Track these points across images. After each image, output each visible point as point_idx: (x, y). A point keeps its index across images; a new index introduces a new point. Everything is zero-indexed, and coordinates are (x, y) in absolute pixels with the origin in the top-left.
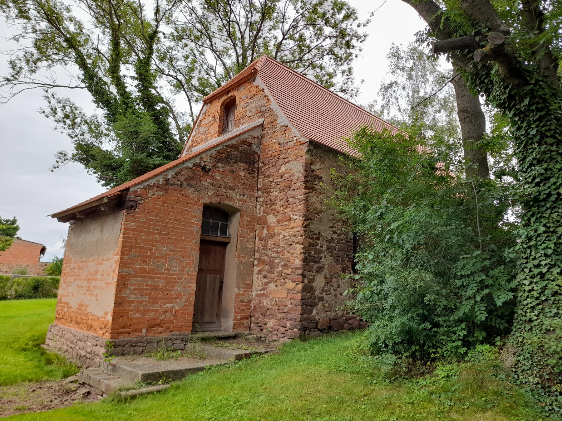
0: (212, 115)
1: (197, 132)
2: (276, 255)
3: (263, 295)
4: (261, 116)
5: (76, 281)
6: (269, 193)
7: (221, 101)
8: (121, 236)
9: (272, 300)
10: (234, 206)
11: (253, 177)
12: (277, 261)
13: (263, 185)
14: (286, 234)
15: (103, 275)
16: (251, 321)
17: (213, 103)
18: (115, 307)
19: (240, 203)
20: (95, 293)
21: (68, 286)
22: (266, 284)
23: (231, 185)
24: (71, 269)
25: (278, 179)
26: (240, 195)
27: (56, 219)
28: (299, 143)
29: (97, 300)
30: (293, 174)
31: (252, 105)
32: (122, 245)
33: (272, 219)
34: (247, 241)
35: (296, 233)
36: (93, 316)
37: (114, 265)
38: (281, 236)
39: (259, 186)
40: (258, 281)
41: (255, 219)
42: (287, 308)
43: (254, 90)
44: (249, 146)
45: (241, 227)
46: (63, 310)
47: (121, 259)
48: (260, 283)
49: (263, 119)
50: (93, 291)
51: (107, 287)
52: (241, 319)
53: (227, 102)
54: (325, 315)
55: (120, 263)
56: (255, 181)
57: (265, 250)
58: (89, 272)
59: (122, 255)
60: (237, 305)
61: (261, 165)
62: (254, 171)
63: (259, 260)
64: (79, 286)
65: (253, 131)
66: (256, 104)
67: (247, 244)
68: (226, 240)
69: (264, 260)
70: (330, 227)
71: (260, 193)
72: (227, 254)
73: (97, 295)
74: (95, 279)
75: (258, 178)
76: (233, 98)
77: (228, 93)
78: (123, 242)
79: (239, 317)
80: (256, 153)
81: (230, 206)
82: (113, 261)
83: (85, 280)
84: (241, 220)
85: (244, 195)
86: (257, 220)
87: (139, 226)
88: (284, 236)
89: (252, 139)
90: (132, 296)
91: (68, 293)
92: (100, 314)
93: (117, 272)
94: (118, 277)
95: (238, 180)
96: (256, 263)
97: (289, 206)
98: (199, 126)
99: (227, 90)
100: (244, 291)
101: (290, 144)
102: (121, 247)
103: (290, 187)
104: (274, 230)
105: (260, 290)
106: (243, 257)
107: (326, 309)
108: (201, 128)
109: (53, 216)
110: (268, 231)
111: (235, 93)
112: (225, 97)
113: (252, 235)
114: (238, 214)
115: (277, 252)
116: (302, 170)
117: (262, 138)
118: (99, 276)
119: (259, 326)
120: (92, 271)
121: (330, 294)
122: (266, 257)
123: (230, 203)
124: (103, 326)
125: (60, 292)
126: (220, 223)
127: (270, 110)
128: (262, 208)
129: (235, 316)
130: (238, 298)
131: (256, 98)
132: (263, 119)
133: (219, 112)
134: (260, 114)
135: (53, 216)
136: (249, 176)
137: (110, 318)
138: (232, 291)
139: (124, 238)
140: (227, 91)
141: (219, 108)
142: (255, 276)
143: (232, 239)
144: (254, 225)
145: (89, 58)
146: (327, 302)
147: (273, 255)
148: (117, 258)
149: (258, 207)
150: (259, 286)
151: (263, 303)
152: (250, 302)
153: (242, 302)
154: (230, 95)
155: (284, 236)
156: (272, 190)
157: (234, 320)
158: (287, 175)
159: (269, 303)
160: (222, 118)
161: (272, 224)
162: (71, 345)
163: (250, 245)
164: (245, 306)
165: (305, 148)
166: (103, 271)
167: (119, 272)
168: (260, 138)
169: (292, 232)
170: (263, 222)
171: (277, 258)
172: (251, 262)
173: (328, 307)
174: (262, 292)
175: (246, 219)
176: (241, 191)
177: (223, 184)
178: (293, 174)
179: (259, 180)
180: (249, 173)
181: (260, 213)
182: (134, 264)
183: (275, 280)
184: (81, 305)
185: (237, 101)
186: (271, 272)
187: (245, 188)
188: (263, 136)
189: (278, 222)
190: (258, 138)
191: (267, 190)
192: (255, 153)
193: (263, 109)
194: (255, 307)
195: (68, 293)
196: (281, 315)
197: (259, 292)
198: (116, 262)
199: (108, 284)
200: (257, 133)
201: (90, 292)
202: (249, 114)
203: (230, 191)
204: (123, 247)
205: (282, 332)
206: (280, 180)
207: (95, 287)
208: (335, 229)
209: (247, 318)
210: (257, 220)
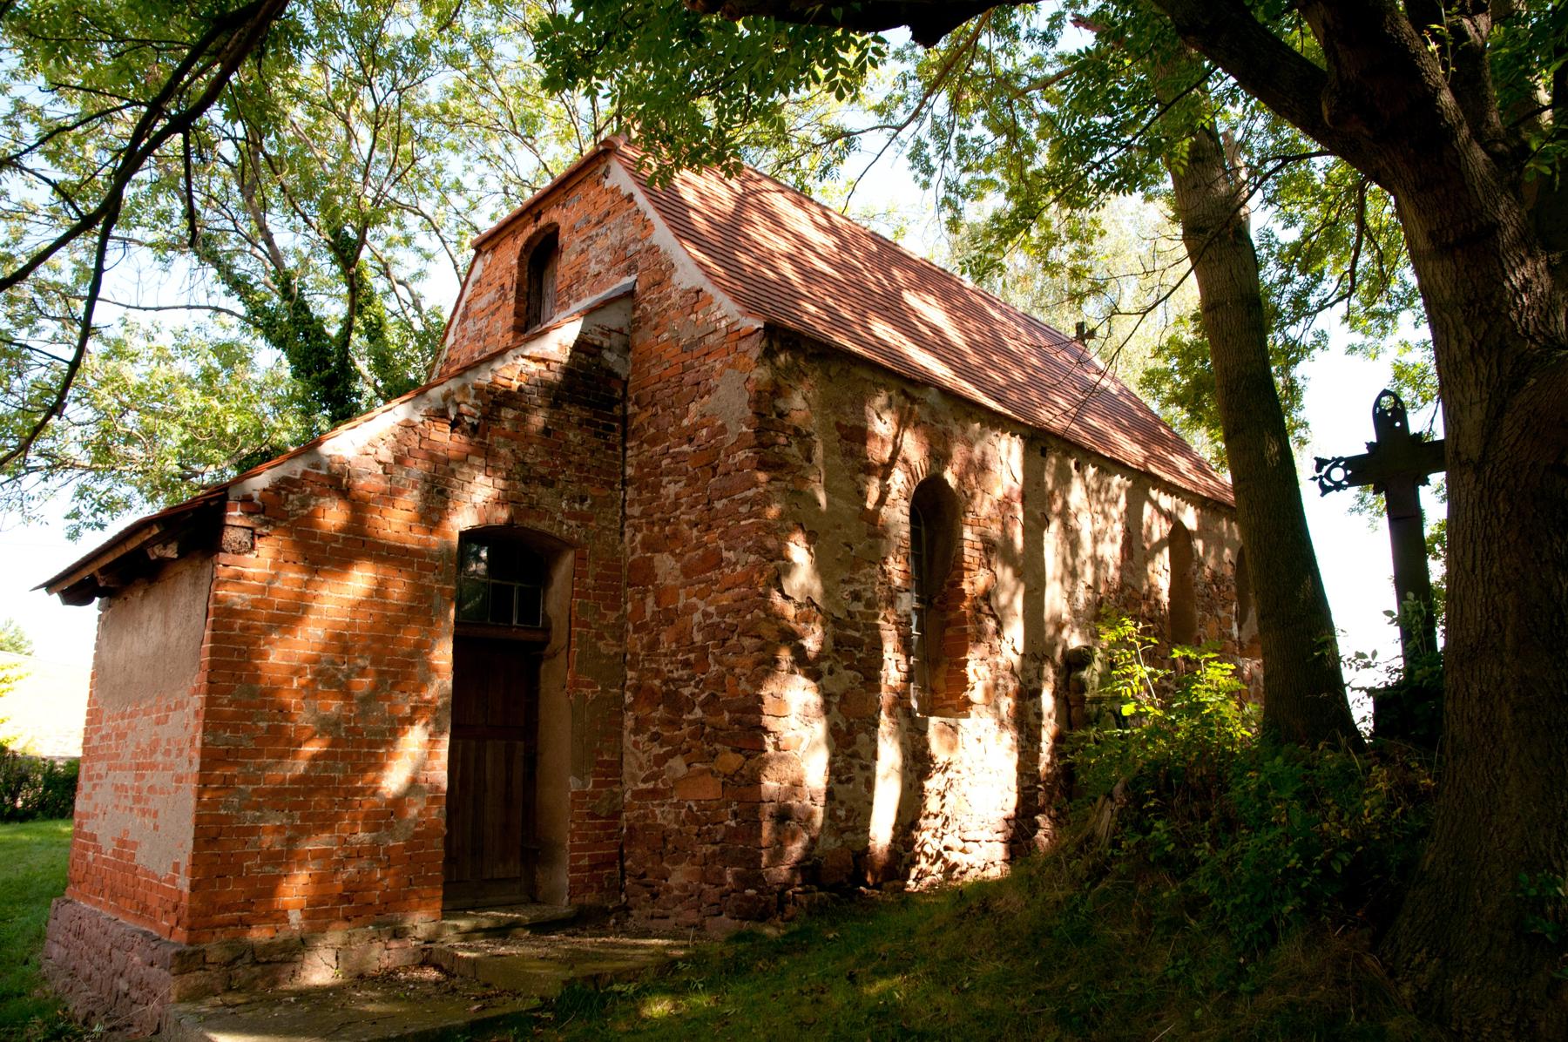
0: (497, 284)
1: (459, 335)
2: (684, 673)
3: (654, 793)
4: (628, 272)
5: (112, 773)
6: (656, 487)
7: (520, 242)
8: (208, 633)
9: (678, 805)
10: (555, 531)
11: (613, 447)
12: (686, 692)
13: (640, 467)
14: (711, 609)
15: (167, 753)
16: (623, 869)
17: (499, 251)
18: (196, 847)
19: (573, 523)
20: (152, 806)
21: (94, 786)
22: (661, 760)
23: (543, 470)
24: (102, 738)
25: (680, 445)
26: (572, 499)
27: (56, 597)
28: (734, 337)
29: (156, 828)
30: (723, 429)
31: (602, 242)
32: (211, 662)
33: (666, 565)
34: (600, 637)
35: (738, 605)
36: (147, 874)
37: (193, 722)
38: (697, 617)
39: (630, 471)
40: (637, 753)
41: (619, 568)
42: (721, 828)
43: (605, 203)
44: (593, 356)
45: (578, 595)
46: (84, 856)
47: (210, 701)
48: (644, 758)
49: (634, 277)
50: (147, 801)
51: (177, 788)
52: (592, 867)
53: (536, 243)
54: (839, 843)
55: (207, 715)
56: (617, 458)
57: (652, 661)
58: (138, 746)
59: (210, 692)
60: (579, 826)
61: (631, 409)
62: (612, 429)
63: (637, 689)
64: (117, 788)
65: (604, 312)
66: (614, 238)
67: (601, 644)
68: (539, 637)
69: (652, 691)
70: (843, 581)
71: (631, 492)
72: (542, 678)
73: (155, 814)
74: (153, 766)
75: (625, 449)
76: (551, 230)
77: (537, 218)
78: (213, 652)
79: (585, 862)
80: (617, 376)
81: (542, 534)
82: (189, 710)
83: (130, 768)
84: (578, 574)
85: (583, 500)
86: (625, 571)
87: (259, 601)
88: (706, 615)
89: (603, 334)
90: (249, 813)
91: (96, 806)
92: (164, 870)
93: (198, 744)
94: (203, 756)
95: (563, 455)
96: (628, 698)
97: (714, 524)
98: (465, 317)
99: (535, 211)
100: (596, 784)
101: (711, 339)
102: (206, 666)
103: (714, 469)
104: (676, 598)
105: (644, 781)
106: (589, 685)
107: (842, 825)
108: (469, 323)
109: (50, 586)
110: (657, 603)
111: (554, 215)
112: (530, 230)
113: (612, 617)
114: (569, 559)
115: (686, 664)
116: (749, 413)
117: (635, 331)
118: (159, 758)
119: (646, 886)
120: (144, 742)
121: (849, 780)
122: (657, 682)
123: (543, 525)
124: (169, 907)
125: (80, 805)
126: (517, 585)
127: (653, 250)
128: (639, 537)
129: (573, 859)
130: (582, 805)
131: (612, 222)
132: (634, 277)
133: (515, 271)
134: (623, 265)
135: (50, 586)
136: (595, 442)
137: (184, 883)
138: (567, 786)
139: (214, 639)
140: (533, 210)
141: (515, 262)
142: (628, 739)
143: (553, 634)
144: (618, 588)
145: (1084, 772)
146: (842, 803)
147: (676, 675)
148: (197, 702)
149: (628, 533)
150: (641, 767)
151: (655, 817)
152: (616, 815)
153: (593, 816)
154: (543, 221)
155: (706, 615)
156: (665, 480)
157: (572, 870)
158: (704, 432)
159: (670, 817)
160: (525, 288)
161: (670, 582)
162: (97, 961)
163: (606, 647)
164: (604, 827)
165: (754, 349)
166: (169, 742)
167: (204, 744)
168: (626, 331)
169: (726, 600)
170: (643, 574)
171: (686, 682)
172: (615, 697)
173: (847, 819)
174: (650, 785)
175: (592, 569)
176: (574, 489)
177: (518, 468)
178: (723, 426)
179: (629, 453)
180: (597, 435)
181: (633, 551)
182: (249, 717)
183: (684, 746)
184: (122, 843)
185: (564, 238)
186: (674, 723)
187: (587, 479)
188: (636, 325)
189: (687, 572)
190: (620, 332)
191: (649, 481)
192: (611, 374)
193: (632, 248)
194: (630, 828)
195: (96, 806)
196: (709, 849)
197: (642, 786)
198: (197, 714)
199: (179, 779)
200: (614, 319)
201: (142, 805)
202: (594, 268)
203: (540, 490)
204: (214, 666)
205: (712, 899)
206: (685, 448)
207: (151, 789)
208: (858, 587)
209: (612, 864)
210: (625, 571)
